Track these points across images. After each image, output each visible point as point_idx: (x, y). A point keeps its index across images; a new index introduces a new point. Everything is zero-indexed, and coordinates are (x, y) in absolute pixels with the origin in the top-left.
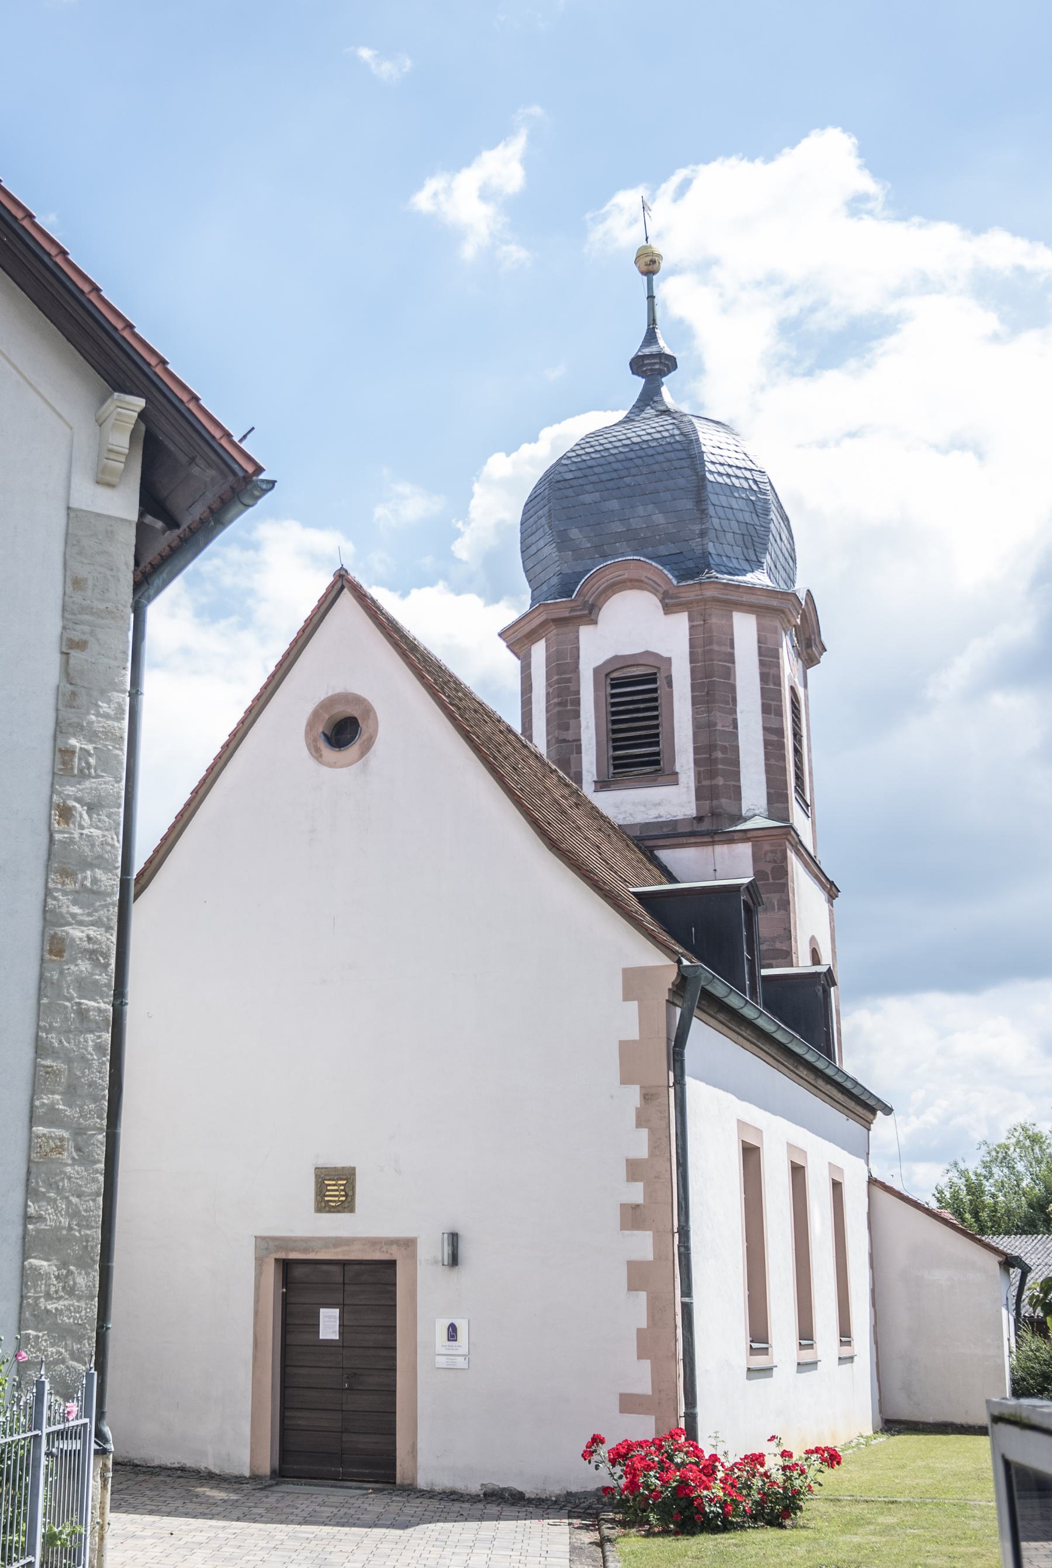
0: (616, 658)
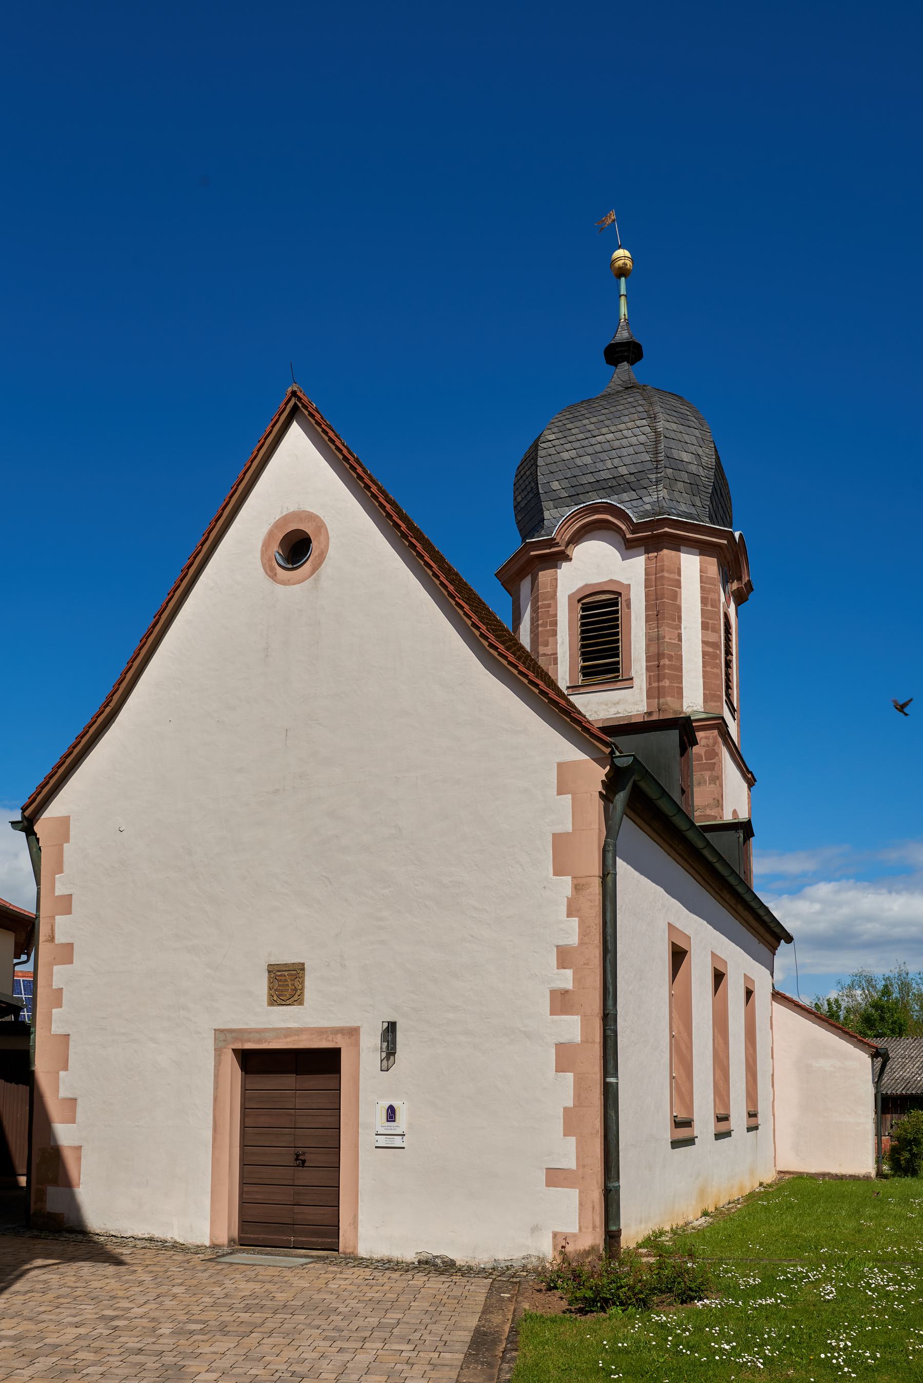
0: (586, 585)
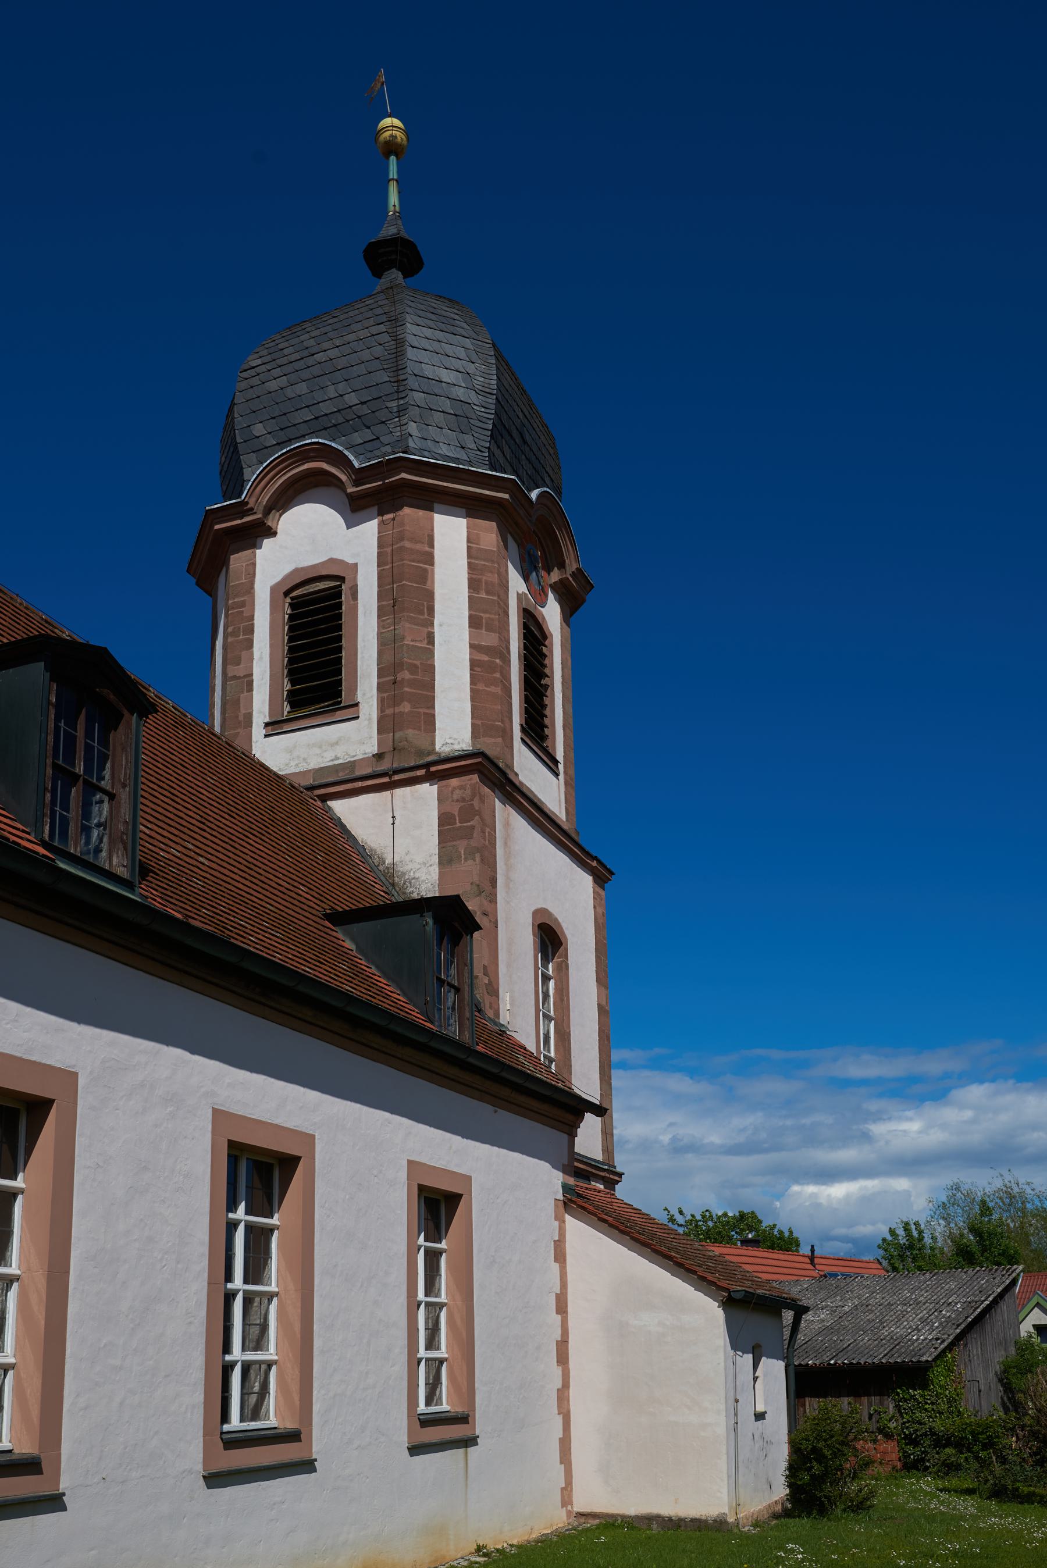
0: (297, 571)
